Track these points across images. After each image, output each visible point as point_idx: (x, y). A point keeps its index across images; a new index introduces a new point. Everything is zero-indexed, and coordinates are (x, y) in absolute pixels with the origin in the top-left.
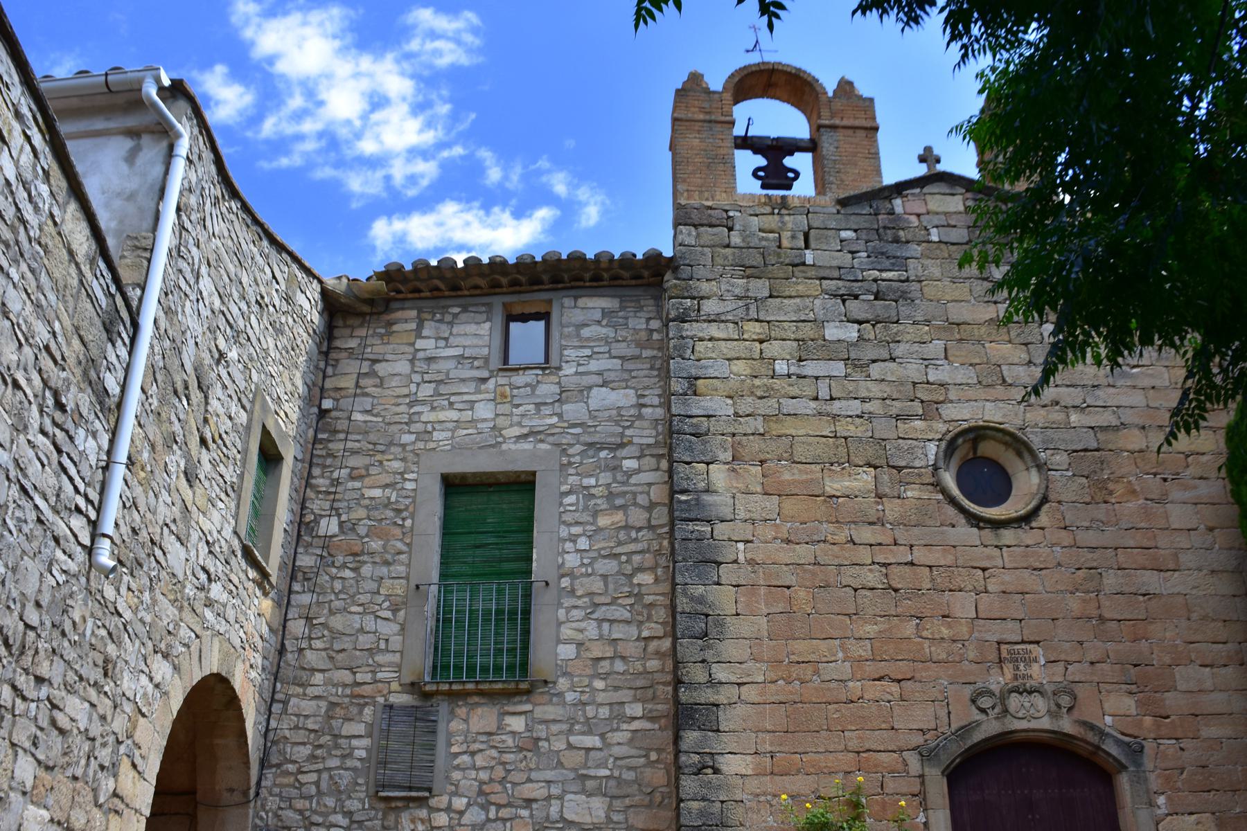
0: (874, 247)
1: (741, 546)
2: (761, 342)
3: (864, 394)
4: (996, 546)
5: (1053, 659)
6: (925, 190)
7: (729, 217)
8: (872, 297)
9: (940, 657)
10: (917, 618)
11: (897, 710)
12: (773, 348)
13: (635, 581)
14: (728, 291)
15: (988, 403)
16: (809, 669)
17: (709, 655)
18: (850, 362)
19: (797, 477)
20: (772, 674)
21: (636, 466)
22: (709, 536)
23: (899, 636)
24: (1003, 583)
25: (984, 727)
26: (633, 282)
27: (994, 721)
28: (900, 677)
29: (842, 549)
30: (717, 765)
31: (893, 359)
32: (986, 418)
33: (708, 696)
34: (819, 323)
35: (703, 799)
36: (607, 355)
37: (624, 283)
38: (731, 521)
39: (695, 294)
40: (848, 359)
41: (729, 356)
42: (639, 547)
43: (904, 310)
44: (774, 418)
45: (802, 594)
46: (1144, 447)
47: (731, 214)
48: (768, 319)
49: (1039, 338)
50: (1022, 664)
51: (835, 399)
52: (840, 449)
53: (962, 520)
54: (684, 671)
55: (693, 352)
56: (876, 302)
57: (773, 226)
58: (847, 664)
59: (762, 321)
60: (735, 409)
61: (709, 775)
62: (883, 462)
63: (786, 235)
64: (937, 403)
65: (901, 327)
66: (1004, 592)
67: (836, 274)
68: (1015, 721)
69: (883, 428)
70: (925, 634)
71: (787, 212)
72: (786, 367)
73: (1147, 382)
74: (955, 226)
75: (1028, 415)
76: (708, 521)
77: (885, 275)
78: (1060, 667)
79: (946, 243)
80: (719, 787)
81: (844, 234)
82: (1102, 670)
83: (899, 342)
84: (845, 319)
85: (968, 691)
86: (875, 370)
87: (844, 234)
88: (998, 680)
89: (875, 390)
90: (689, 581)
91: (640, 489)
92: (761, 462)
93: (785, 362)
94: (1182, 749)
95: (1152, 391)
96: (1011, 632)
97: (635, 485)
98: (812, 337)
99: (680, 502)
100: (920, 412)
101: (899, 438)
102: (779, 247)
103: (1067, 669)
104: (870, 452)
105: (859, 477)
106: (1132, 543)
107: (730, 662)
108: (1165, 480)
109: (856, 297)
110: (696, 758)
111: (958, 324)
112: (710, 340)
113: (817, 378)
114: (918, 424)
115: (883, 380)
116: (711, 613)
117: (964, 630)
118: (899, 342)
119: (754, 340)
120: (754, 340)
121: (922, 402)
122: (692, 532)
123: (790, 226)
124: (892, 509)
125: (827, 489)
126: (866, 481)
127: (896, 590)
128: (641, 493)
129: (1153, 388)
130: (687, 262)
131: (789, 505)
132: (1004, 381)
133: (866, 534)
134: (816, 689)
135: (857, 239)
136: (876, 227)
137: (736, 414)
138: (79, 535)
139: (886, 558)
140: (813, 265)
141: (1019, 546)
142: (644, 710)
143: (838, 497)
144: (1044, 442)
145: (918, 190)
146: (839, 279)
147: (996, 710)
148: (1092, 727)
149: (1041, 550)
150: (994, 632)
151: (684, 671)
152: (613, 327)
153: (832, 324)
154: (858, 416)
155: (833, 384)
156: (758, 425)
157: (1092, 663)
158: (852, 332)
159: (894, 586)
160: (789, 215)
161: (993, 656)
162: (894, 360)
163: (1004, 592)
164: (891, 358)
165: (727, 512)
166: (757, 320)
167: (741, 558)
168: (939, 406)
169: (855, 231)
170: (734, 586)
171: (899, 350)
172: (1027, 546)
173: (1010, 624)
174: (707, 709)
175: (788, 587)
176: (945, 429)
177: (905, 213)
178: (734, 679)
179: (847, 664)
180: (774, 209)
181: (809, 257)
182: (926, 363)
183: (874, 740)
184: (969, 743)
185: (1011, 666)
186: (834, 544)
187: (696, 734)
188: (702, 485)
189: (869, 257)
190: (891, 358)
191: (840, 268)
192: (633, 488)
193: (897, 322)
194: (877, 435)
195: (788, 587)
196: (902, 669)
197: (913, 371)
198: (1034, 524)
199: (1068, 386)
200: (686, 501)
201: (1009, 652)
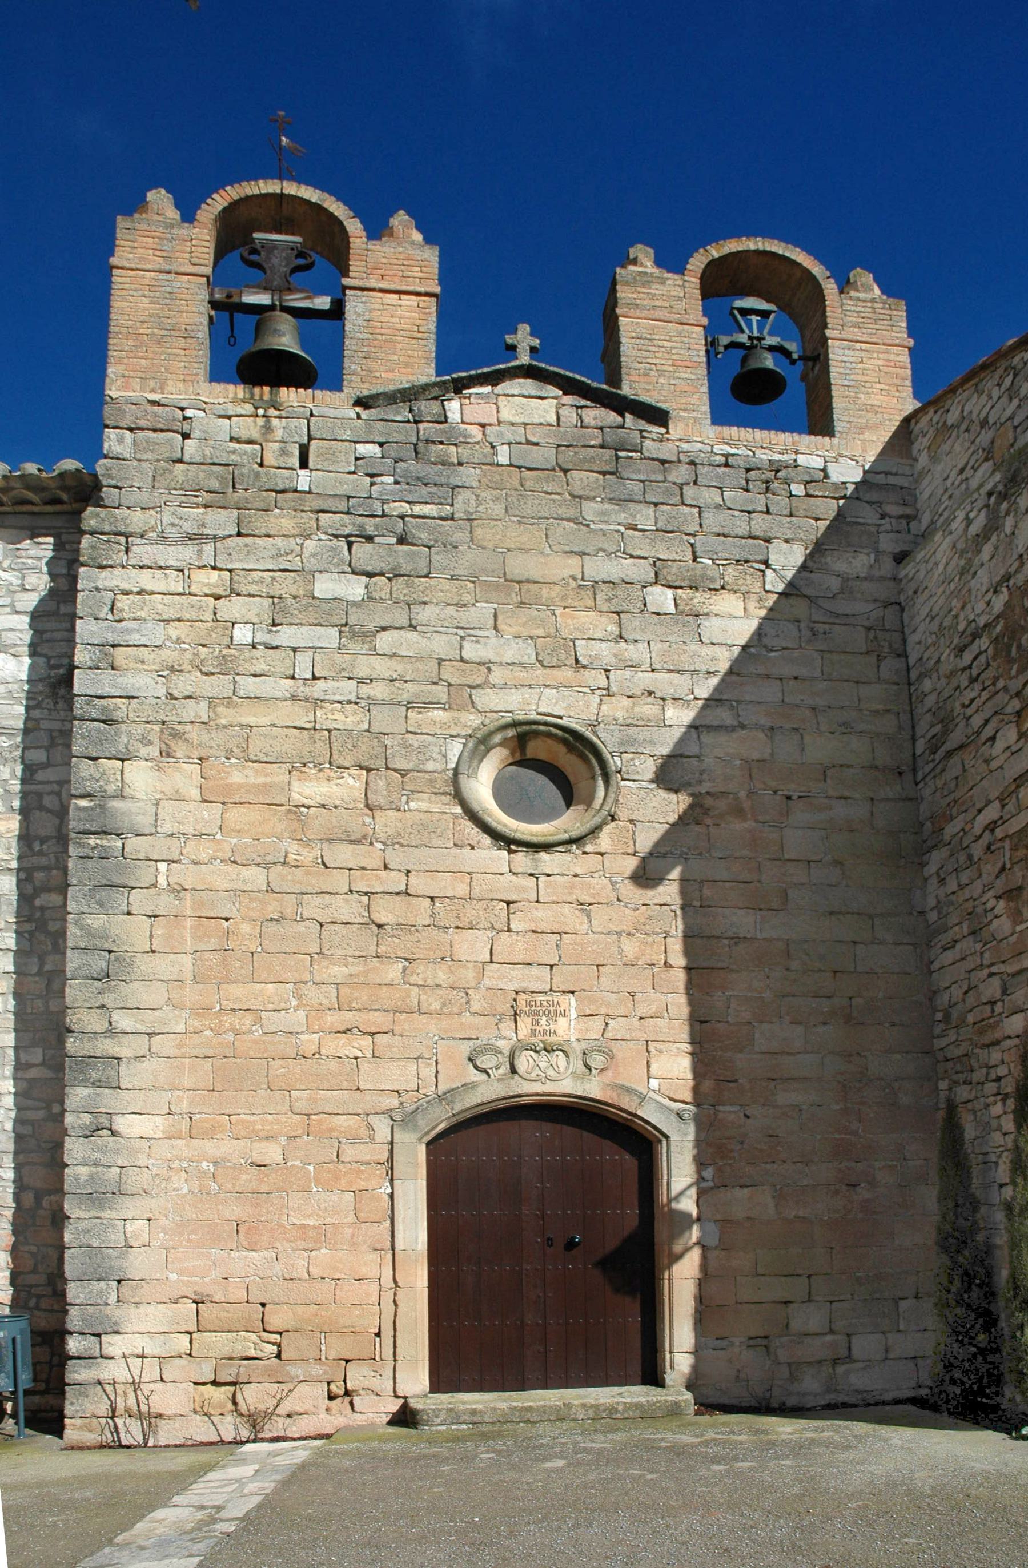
0: (407, 470)
1: (163, 866)
2: (218, 598)
3: (362, 672)
4: (531, 875)
5: (588, 1012)
6: (499, 389)
7: (185, 418)
8: (394, 540)
9: (432, 1008)
10: (406, 960)
11: (364, 1066)
12: (232, 608)
13: (38, 902)
14: (173, 525)
15: (547, 691)
16: (248, 1019)
17: (109, 999)
18: (347, 629)
19: (252, 780)
20: (196, 1024)
21: (44, 759)
22: (118, 853)
23: (378, 981)
24: (532, 920)
25: (481, 1090)
26: (49, 509)
27: (496, 1084)
28: (374, 1030)
29: (308, 873)
30: (114, 1127)
31: (413, 627)
32: (541, 710)
33: (107, 1046)
34: (308, 575)
35: (96, 1164)
36: (8, 610)
37: (36, 509)
38: (151, 835)
39: (122, 528)
40: (346, 624)
41: (165, 617)
42: (44, 861)
43: (439, 558)
44: (225, 702)
45: (245, 928)
46: (766, 756)
47: (189, 413)
48: (229, 567)
49: (640, 605)
50: (544, 1018)
51: (319, 678)
52: (317, 745)
53: (487, 840)
54: (75, 1018)
55: (112, 609)
56: (400, 547)
57: (256, 435)
58: (301, 1014)
59: (221, 569)
60: (168, 688)
61: (104, 1139)
62: (380, 763)
63: (272, 449)
64: (471, 687)
65: (432, 582)
66: (534, 931)
67: (342, 506)
68: (525, 1083)
69: (384, 720)
70: (413, 979)
71: (277, 413)
72: (250, 634)
73: (787, 670)
74: (537, 444)
75: (604, 707)
76: (118, 835)
77: (418, 510)
78: (598, 1023)
79: (519, 467)
80: (117, 1152)
81: (362, 449)
82: (656, 1025)
83: (425, 603)
84: (349, 570)
85: (466, 1047)
86: (385, 641)
87: (362, 449)
88: (506, 1036)
89: (382, 667)
90: (86, 909)
91: (48, 788)
92: (200, 759)
93: (250, 626)
94: (747, 1116)
95: (792, 682)
96: (537, 978)
97: (41, 783)
98: (294, 593)
99: (79, 809)
100: (444, 698)
101: (408, 732)
102: (261, 465)
103: (607, 1024)
104: (365, 751)
105: (341, 781)
106: (725, 875)
107: (138, 1008)
108: (789, 798)
109: (370, 539)
110: (87, 1119)
111: (519, 582)
112: (139, 593)
113: (294, 650)
114: (438, 715)
115: (395, 655)
116: (115, 949)
117: (469, 975)
118: (425, 603)
119: (206, 595)
120: (206, 595)
121: (450, 685)
122: (93, 848)
123: (279, 434)
124: (386, 822)
125: (295, 796)
126: (352, 787)
127: (380, 926)
128: (49, 794)
129: (796, 678)
130: (113, 482)
131: (236, 816)
132: (577, 661)
133: (344, 854)
134: (255, 1042)
135: (383, 457)
136: (414, 440)
137: (171, 697)
138: (550, 711)
139: (369, 886)
140: (310, 492)
141: (563, 875)
142: (44, 1055)
143: (308, 807)
144: (622, 743)
145: (488, 389)
146: (348, 513)
147: (501, 1071)
148: (629, 1091)
149: (595, 881)
150: (515, 979)
151: (75, 1018)
152: (20, 570)
153: (326, 576)
154: (350, 702)
155: (317, 657)
156: (201, 710)
157: (641, 1018)
158: (355, 589)
159: (378, 921)
160: (280, 417)
161: (505, 1008)
162: (415, 627)
163: (534, 931)
164: (411, 625)
165: (144, 822)
166: (214, 568)
167: (162, 881)
168: (474, 691)
169: (381, 445)
170: (150, 917)
171: (424, 615)
172: (576, 876)
173: (535, 970)
174: (103, 1063)
175: (227, 919)
176: (478, 722)
177: (463, 422)
178: (142, 1028)
179: (301, 1014)
180: (256, 408)
181: (303, 480)
182: (461, 632)
183: (330, 1099)
184: (458, 1107)
185: (529, 1020)
186: (297, 867)
187: (87, 1091)
188: (111, 788)
189: (397, 483)
190: (411, 625)
191: (349, 497)
192: (39, 787)
193: (426, 576)
194: (375, 729)
195: (227, 919)
196: (379, 1020)
197: (441, 645)
198: (589, 848)
199: (670, 671)
200: (85, 809)
201: (528, 1004)
